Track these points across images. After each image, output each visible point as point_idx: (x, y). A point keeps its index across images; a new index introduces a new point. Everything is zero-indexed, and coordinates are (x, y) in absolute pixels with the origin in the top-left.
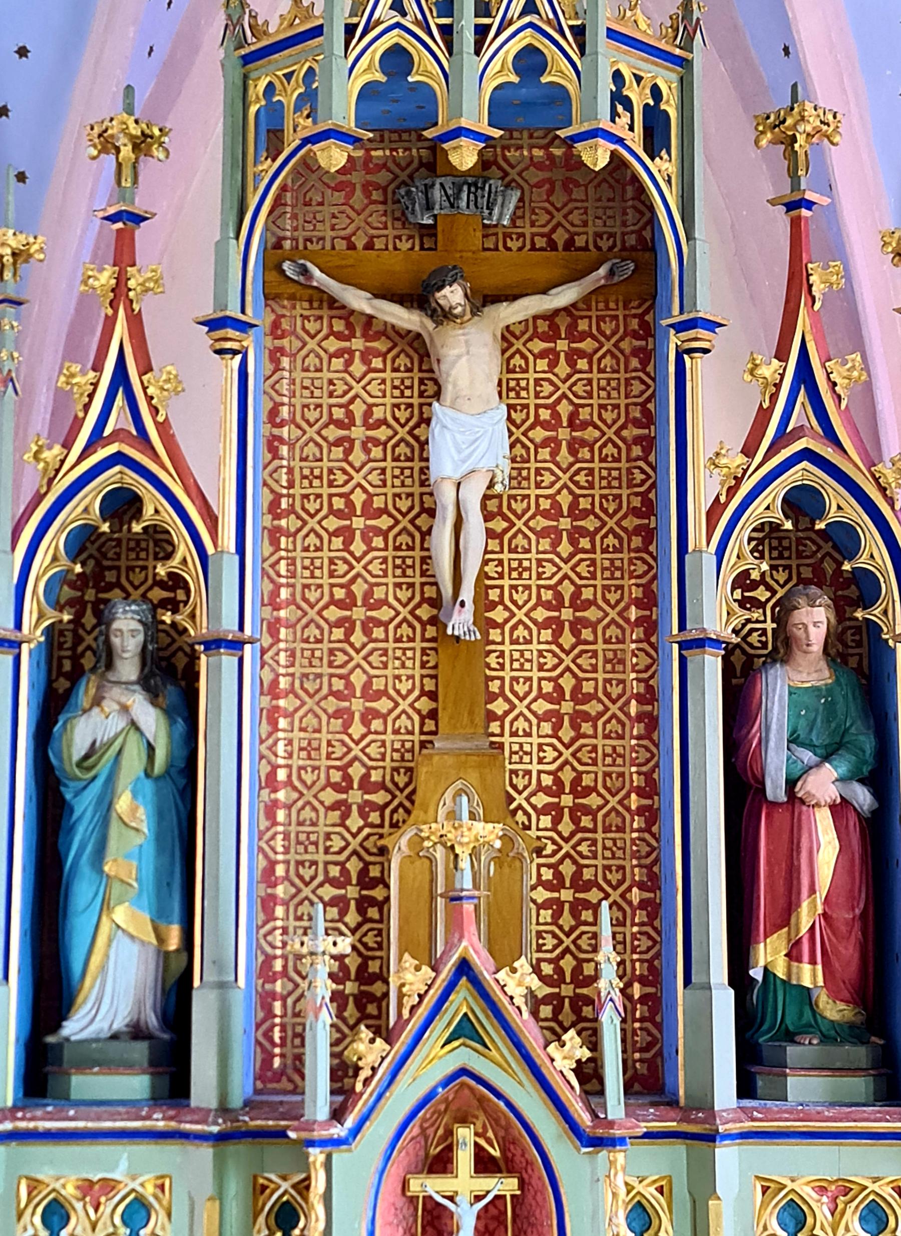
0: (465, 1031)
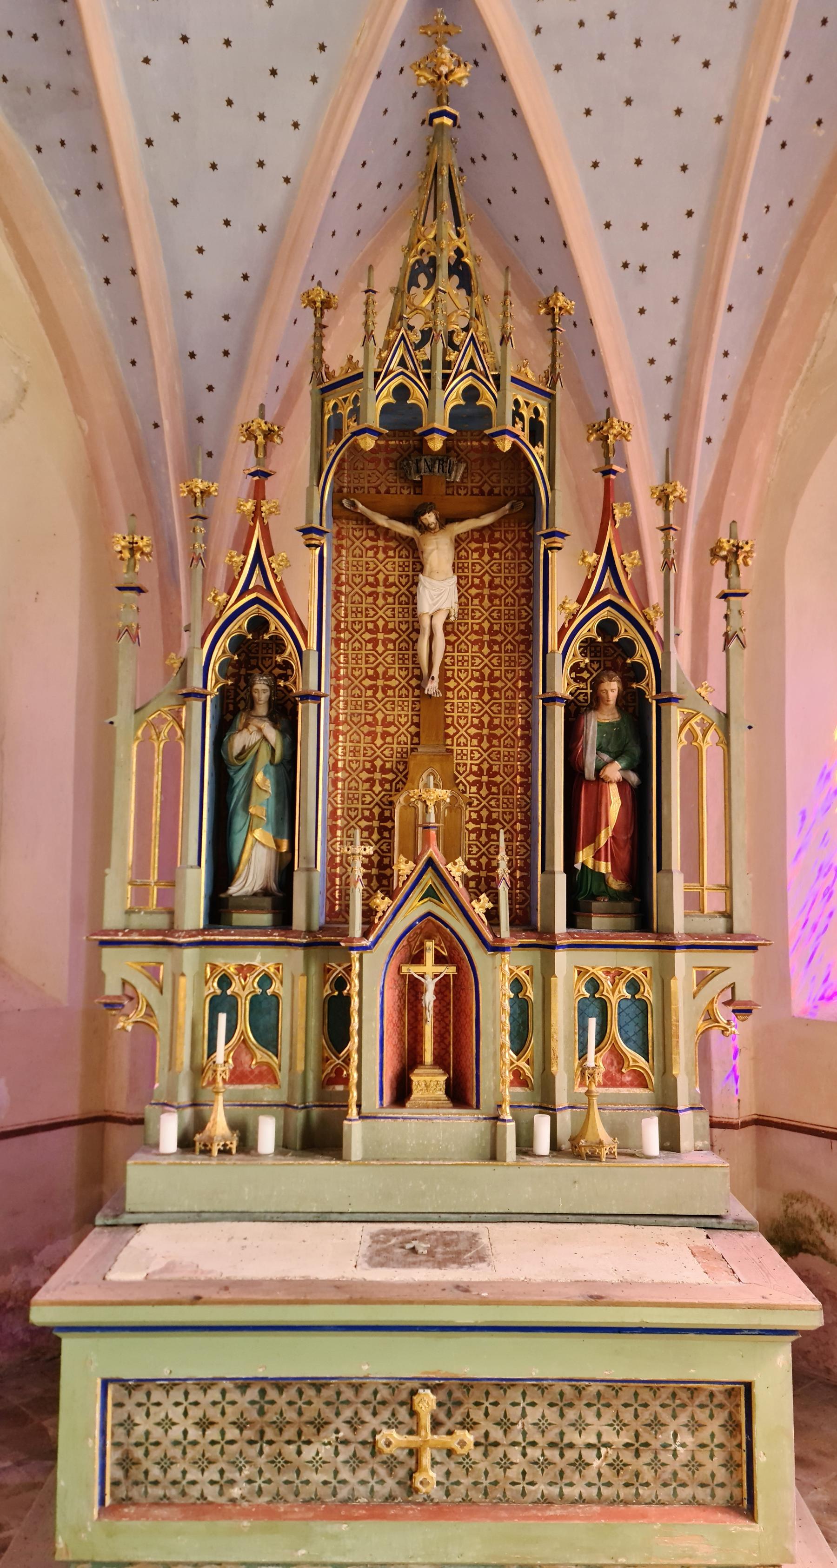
0: (431, 893)
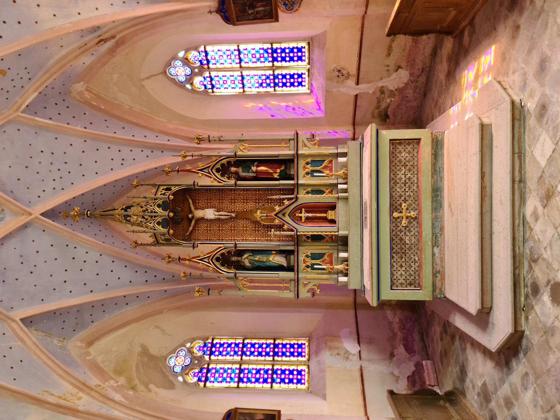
0: (284, 215)
